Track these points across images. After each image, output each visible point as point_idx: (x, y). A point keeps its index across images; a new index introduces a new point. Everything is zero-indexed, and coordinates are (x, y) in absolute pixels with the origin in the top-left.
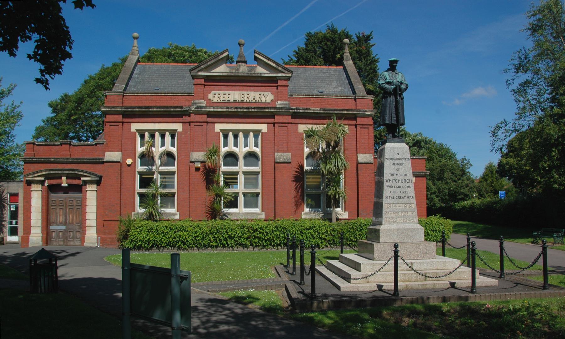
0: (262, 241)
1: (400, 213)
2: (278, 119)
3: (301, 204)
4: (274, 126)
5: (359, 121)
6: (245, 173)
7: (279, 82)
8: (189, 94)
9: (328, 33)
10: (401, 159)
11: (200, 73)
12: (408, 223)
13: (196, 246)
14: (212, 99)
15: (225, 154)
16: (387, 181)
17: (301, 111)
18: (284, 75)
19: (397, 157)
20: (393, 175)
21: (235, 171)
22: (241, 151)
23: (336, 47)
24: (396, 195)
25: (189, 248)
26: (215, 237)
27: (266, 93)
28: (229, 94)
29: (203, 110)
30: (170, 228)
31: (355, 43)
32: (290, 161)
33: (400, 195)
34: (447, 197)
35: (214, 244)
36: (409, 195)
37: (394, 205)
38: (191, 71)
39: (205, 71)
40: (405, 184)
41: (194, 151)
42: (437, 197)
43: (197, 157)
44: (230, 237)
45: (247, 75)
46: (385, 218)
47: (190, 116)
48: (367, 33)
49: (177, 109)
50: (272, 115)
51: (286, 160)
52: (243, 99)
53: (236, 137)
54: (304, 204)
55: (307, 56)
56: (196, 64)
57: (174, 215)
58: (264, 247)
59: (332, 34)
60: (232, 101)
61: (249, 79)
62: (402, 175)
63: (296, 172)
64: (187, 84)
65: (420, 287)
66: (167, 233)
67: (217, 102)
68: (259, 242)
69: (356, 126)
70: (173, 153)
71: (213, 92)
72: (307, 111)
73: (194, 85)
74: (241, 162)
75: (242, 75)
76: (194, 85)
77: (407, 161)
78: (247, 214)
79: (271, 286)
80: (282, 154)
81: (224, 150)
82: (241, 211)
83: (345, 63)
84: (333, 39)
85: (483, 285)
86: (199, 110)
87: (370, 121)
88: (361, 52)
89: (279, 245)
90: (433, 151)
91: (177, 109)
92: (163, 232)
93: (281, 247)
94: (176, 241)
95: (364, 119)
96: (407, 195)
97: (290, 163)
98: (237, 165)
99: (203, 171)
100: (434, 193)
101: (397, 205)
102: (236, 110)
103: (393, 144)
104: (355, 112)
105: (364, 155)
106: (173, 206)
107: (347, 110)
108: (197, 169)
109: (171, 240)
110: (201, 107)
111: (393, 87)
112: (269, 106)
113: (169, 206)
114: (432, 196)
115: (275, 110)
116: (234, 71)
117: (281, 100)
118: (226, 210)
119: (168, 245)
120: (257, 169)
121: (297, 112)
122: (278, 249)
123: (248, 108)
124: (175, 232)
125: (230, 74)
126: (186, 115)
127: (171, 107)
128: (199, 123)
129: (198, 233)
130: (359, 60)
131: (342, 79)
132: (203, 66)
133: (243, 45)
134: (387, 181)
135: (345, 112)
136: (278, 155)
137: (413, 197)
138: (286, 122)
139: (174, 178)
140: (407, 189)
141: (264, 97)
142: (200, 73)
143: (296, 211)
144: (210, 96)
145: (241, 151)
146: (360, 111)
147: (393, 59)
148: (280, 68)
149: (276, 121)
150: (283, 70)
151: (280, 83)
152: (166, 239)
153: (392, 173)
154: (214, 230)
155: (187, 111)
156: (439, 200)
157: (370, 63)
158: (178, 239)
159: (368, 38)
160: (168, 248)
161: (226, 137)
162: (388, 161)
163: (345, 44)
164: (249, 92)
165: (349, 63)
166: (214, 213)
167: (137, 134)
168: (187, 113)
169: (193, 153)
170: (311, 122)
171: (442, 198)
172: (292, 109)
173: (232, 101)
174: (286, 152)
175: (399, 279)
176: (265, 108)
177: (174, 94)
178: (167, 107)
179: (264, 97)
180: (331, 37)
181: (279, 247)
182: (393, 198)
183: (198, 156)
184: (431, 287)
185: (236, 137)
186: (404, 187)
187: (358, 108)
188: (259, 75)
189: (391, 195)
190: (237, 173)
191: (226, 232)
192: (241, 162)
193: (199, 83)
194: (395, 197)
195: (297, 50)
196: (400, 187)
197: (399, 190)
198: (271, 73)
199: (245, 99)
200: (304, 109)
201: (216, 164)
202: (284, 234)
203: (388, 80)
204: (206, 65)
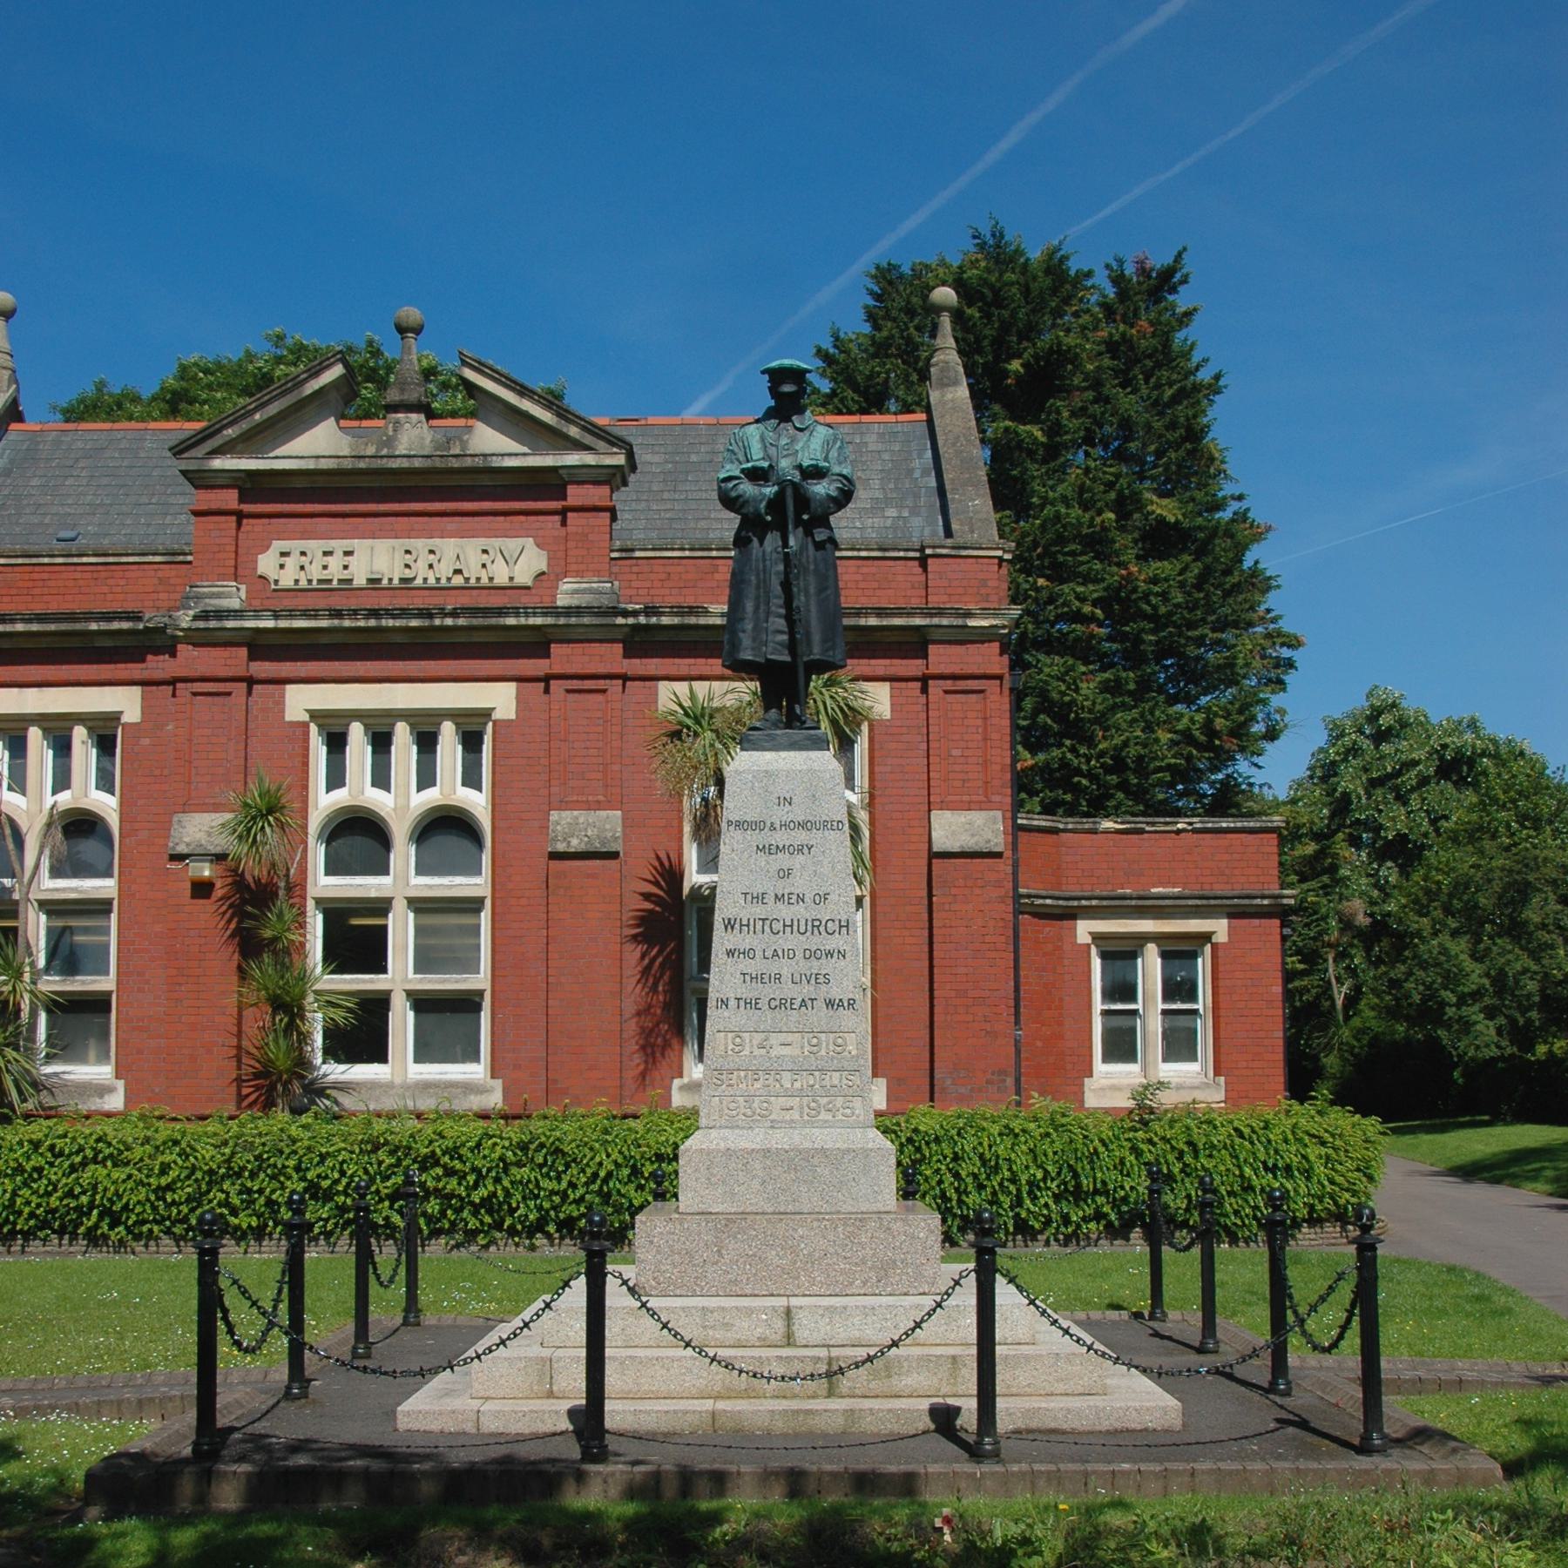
0: (458, 1211)
1: (786, 1078)
2: (563, 657)
3: (666, 1045)
4: (924, 690)
5: (941, 658)
6: (420, 906)
7: (571, 490)
8: (175, 557)
9: (974, 264)
10: (802, 825)
11: (218, 463)
12: (825, 1124)
13: (168, 1232)
14: (272, 576)
15: (330, 818)
16: (729, 925)
17: (665, 620)
18: (589, 459)
19: (781, 814)
20: (760, 898)
21: (373, 894)
22: (401, 805)
23: (1005, 328)
24: (768, 991)
25: (138, 1237)
26: (249, 1191)
27: (511, 545)
28: (348, 553)
29: (230, 624)
30: (52, 1148)
31: (1108, 308)
32: (614, 847)
33: (788, 990)
34: (1534, 1014)
35: (245, 1220)
36: (836, 993)
37: (758, 1037)
38: (179, 450)
39: (241, 454)
40: (815, 941)
41: (188, 807)
42: (1491, 1013)
43: (201, 837)
44: (313, 1189)
45: (427, 463)
47: (173, 655)
48: (1159, 259)
49: (116, 625)
50: (536, 643)
51: (597, 846)
52: (408, 574)
53: (381, 742)
54: (683, 1042)
55: (873, 375)
56: (198, 426)
57: (103, 1090)
58: (471, 1235)
59: (988, 270)
60: (360, 581)
61: (364, 483)
62: (801, 898)
63: (647, 897)
64: (172, 515)
65: (780, 1425)
66: (39, 1170)
67: (295, 591)
68: (443, 1213)
69: (924, 680)
70: (102, 819)
71: (278, 545)
72: (693, 620)
73: (197, 513)
74: (403, 853)
75: (405, 464)
76: (197, 513)
78: (426, 1086)
79: (120, 1403)
80: (582, 816)
81: (324, 802)
82: (402, 1073)
83: (934, 396)
84: (996, 292)
85: (1105, 1425)
86: (213, 624)
87: (990, 659)
88: (1132, 348)
89: (539, 1227)
90: (1495, 800)
91: (116, 625)
92: (19, 1169)
93: (549, 1236)
94: (78, 1209)
95: (960, 649)
96: (823, 992)
97: (614, 855)
98: (385, 871)
99: (224, 898)
100: (1477, 995)
101: (775, 1039)
102: (372, 623)
103: (769, 755)
104: (918, 621)
105: (961, 818)
106: (103, 1058)
107: (880, 612)
108: (202, 889)
109: (54, 1202)
110: (220, 614)
111: (770, 491)
112: (525, 600)
113: (92, 1054)
114: (1465, 1011)
115: (550, 620)
116: (371, 450)
117: (579, 573)
118: (336, 1072)
119: (45, 1224)
120: (476, 885)
121: (647, 627)
122: (533, 1248)
123: (426, 614)
124: (73, 1169)
125: (348, 464)
126: (157, 651)
127: (89, 616)
128: (214, 685)
129: (173, 1174)
130: (1123, 386)
131: (910, 471)
132: (230, 432)
133: (418, 330)
134: (729, 925)
135: (873, 621)
136: (561, 819)
137: (852, 1003)
138: (602, 670)
139: (107, 931)
140: (827, 966)
141: (501, 559)
142: (218, 463)
143: (643, 1075)
144: (266, 564)
145: (401, 805)
146: (940, 612)
147: (787, 362)
148: (573, 431)
149: (933, 670)
150: (588, 439)
151: (576, 495)
152: (35, 1200)
153: (758, 889)
154: (244, 1159)
155: (161, 630)
156: (1499, 1031)
157: (1176, 400)
158: (84, 1199)
159: (1165, 281)
160: (45, 1240)
161: (337, 743)
162: (738, 834)
163: (937, 309)
164: (436, 542)
165: (953, 397)
166: (277, 1083)
167: (313, 728)
168: (159, 642)
169: (185, 818)
170: (684, 671)
171: (1512, 1021)
172: (625, 614)
173: (360, 581)
174: (598, 806)
176: (501, 612)
177: (110, 561)
178: (72, 617)
179: (501, 559)
180: (985, 282)
181: (539, 1240)
182: (753, 1004)
183: (201, 829)
184: (836, 1424)
185: (381, 742)
186: (811, 955)
187: (934, 601)
188: (479, 462)
189: (746, 992)
190: (381, 907)
191: (298, 1169)
192: (403, 853)
193: (214, 506)
194: (763, 1004)
195: (827, 344)
196: (790, 954)
197: (785, 968)
198: (536, 450)
199: (421, 573)
200: (680, 611)
201: (273, 865)
202: (559, 1179)
203: (758, 459)
204: (244, 425)
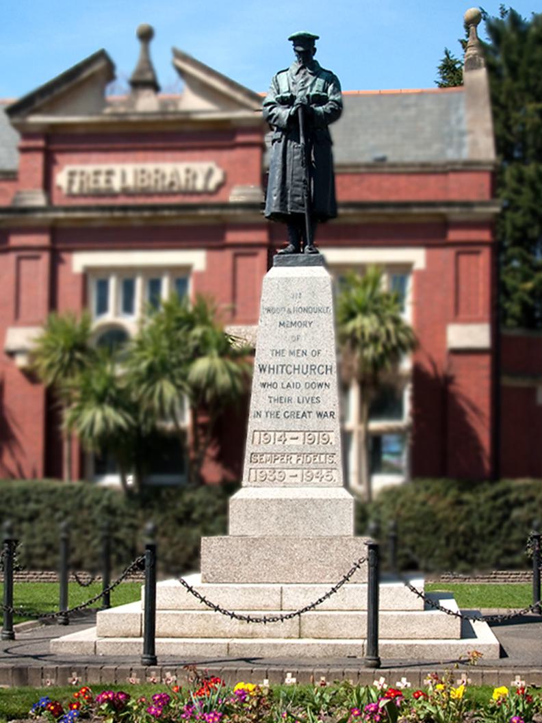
10: (306, 310)
16: (262, 369)
19: (293, 304)
20: (279, 353)
24: (284, 407)
36: (323, 408)
40: (312, 378)
46: (249, 468)
77: (323, 315)
96: (316, 408)
134: (262, 369)
137: (332, 414)
140: (318, 392)
148: (239, 97)
150: (247, 101)
175: (380, 632)
194: (281, 415)
197: (294, 393)
198: (223, 110)
